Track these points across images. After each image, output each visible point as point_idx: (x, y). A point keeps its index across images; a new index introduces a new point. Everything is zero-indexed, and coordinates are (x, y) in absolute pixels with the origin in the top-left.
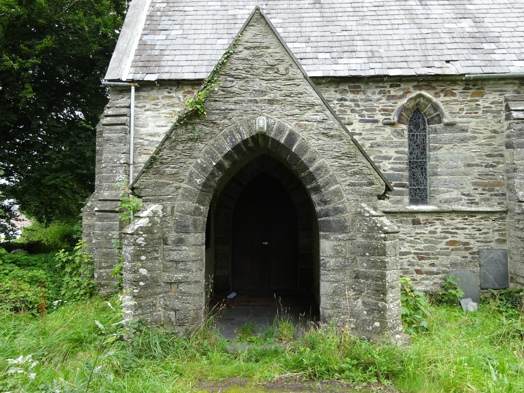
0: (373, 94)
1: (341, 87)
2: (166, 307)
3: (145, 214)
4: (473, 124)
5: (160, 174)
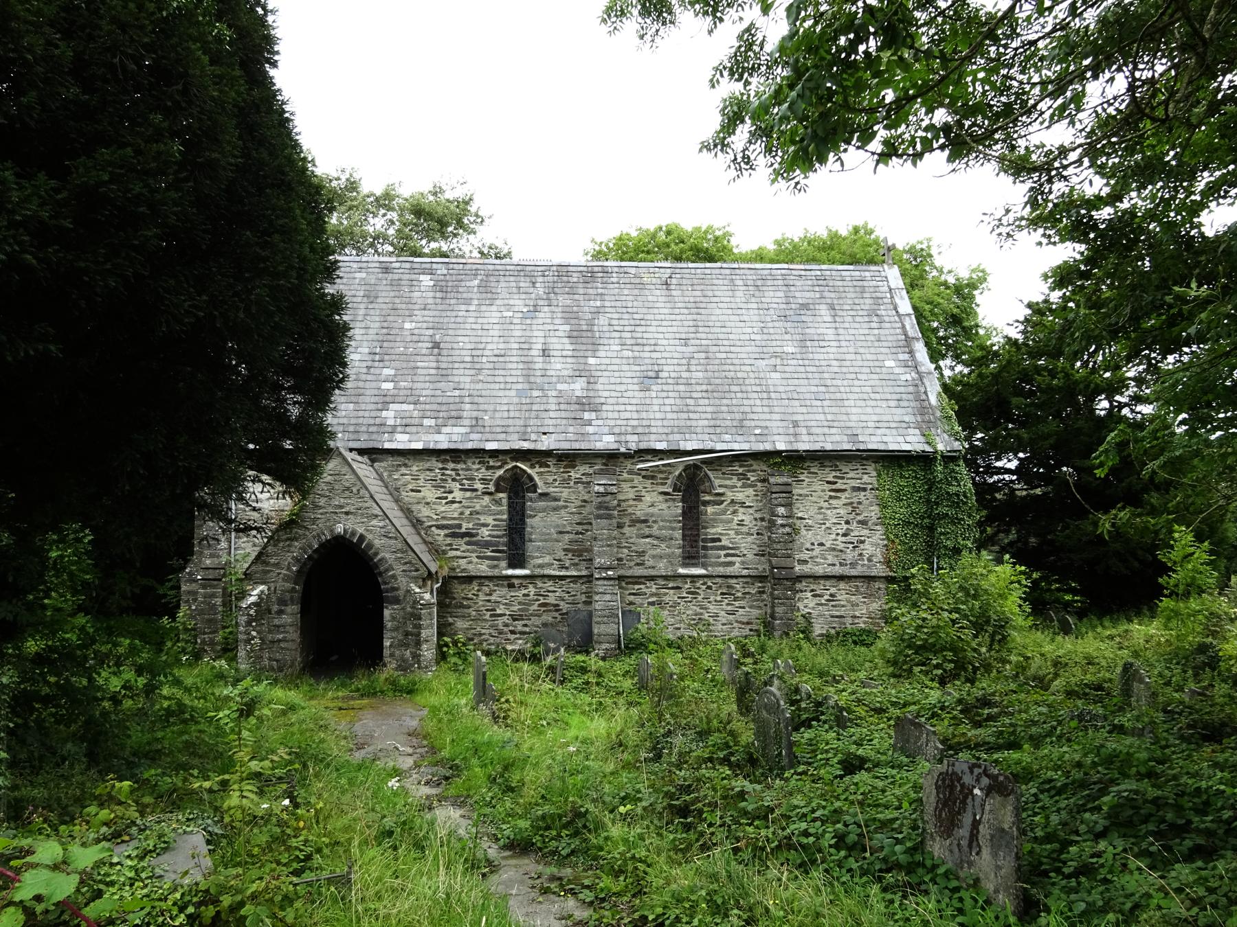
2: (270, 659)
3: (255, 592)
4: (565, 493)
5: (266, 563)
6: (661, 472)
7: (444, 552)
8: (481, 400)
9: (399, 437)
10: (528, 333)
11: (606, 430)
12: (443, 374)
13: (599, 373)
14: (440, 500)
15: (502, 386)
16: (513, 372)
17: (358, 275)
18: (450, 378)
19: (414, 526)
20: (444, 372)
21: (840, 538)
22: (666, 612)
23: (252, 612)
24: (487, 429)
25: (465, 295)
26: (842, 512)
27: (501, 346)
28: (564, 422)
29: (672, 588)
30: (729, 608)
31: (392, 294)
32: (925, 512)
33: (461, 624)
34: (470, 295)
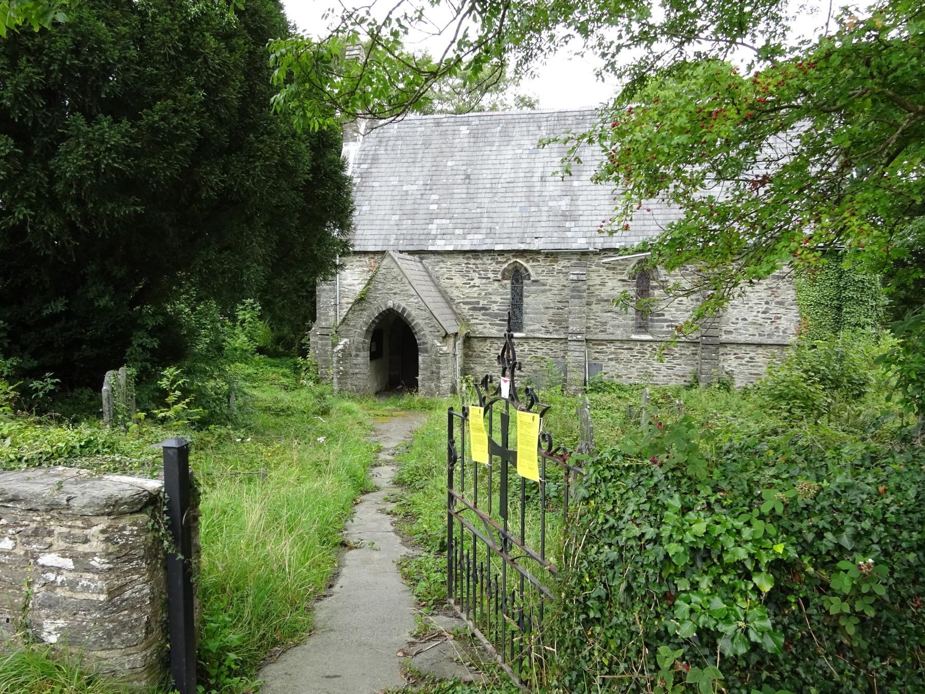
0: (487, 260)
1: (467, 255)
4: (550, 280)
6: (620, 265)
7: (468, 320)
8: (495, 215)
9: (439, 242)
10: (532, 165)
11: (581, 234)
12: (471, 197)
13: (580, 193)
14: (464, 284)
15: (510, 204)
16: (519, 194)
17: (419, 129)
18: (475, 200)
19: (447, 302)
20: (472, 196)
21: (760, 315)
22: (622, 366)
23: (340, 355)
24: (497, 236)
25: (490, 139)
26: (763, 295)
27: (512, 175)
28: (551, 229)
29: (627, 349)
30: (669, 364)
31: (441, 141)
32: (835, 296)
33: (479, 369)
34: (493, 139)
